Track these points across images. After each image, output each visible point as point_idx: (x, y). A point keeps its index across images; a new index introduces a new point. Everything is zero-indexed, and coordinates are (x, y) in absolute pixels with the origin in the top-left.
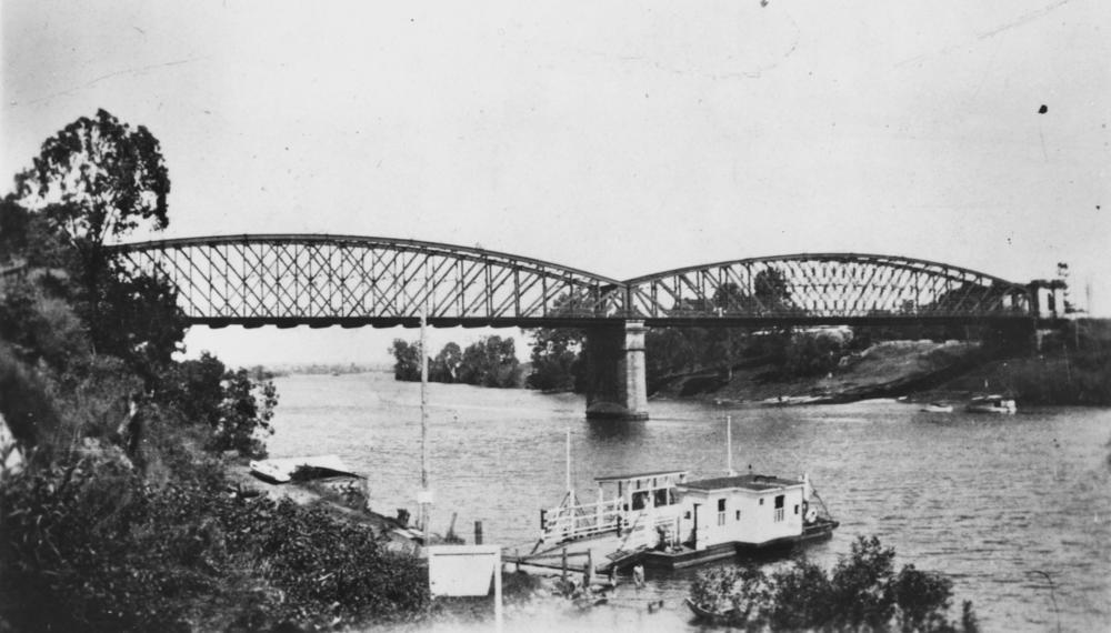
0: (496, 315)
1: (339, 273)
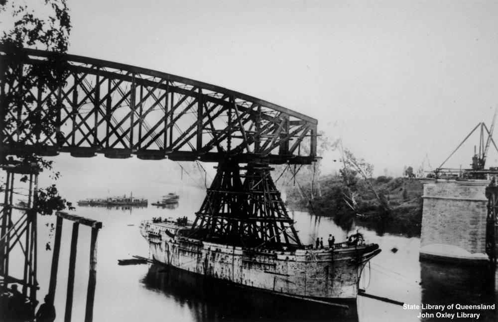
0: (143, 145)
1: (100, 117)
